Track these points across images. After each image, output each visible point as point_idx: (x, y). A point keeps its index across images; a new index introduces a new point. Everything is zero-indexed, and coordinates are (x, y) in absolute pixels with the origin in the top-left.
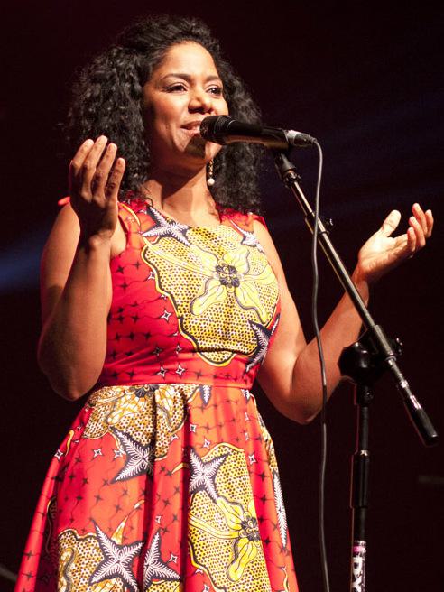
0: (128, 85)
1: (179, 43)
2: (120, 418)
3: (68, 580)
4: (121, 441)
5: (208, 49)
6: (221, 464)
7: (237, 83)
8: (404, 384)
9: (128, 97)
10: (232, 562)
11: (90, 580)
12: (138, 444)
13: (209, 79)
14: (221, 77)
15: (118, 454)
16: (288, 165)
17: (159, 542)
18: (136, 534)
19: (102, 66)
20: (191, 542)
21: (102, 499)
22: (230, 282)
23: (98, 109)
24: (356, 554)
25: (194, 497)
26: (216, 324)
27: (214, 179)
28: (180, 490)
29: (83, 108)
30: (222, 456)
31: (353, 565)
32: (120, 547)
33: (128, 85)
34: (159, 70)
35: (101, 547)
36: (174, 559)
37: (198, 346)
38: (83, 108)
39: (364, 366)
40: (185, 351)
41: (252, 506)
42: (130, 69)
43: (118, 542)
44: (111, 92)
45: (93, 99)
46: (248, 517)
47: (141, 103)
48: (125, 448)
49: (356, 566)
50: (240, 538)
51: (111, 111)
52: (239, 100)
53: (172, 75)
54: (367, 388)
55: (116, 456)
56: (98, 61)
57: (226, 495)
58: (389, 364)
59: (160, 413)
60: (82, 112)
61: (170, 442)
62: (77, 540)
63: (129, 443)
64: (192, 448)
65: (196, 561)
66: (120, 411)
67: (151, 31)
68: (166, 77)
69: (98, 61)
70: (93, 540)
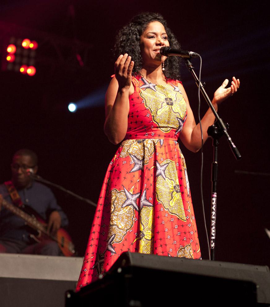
0: (135, 36)
1: (152, 22)
3: (114, 206)
4: (133, 158)
5: (162, 24)
7: (172, 35)
8: (230, 139)
12: (138, 159)
13: (163, 34)
14: (167, 33)
16: (190, 63)
17: (146, 193)
18: (138, 190)
19: (126, 29)
20: (156, 193)
24: (213, 197)
29: (119, 44)
30: (167, 164)
31: (212, 201)
32: (132, 195)
33: (135, 36)
34: (146, 31)
35: (126, 195)
36: (151, 199)
39: (216, 133)
40: (154, 127)
41: (177, 181)
42: (136, 30)
43: (132, 193)
44: (129, 38)
45: (123, 41)
46: (176, 185)
48: (134, 161)
49: (213, 201)
50: (173, 192)
52: (173, 41)
53: (150, 33)
54: (217, 140)
55: (131, 163)
56: (125, 28)
58: (224, 132)
59: (146, 149)
61: (150, 159)
63: (135, 159)
64: (157, 160)
66: (132, 148)
67: (143, 17)
68: (148, 33)
69: (125, 28)
70: (123, 192)
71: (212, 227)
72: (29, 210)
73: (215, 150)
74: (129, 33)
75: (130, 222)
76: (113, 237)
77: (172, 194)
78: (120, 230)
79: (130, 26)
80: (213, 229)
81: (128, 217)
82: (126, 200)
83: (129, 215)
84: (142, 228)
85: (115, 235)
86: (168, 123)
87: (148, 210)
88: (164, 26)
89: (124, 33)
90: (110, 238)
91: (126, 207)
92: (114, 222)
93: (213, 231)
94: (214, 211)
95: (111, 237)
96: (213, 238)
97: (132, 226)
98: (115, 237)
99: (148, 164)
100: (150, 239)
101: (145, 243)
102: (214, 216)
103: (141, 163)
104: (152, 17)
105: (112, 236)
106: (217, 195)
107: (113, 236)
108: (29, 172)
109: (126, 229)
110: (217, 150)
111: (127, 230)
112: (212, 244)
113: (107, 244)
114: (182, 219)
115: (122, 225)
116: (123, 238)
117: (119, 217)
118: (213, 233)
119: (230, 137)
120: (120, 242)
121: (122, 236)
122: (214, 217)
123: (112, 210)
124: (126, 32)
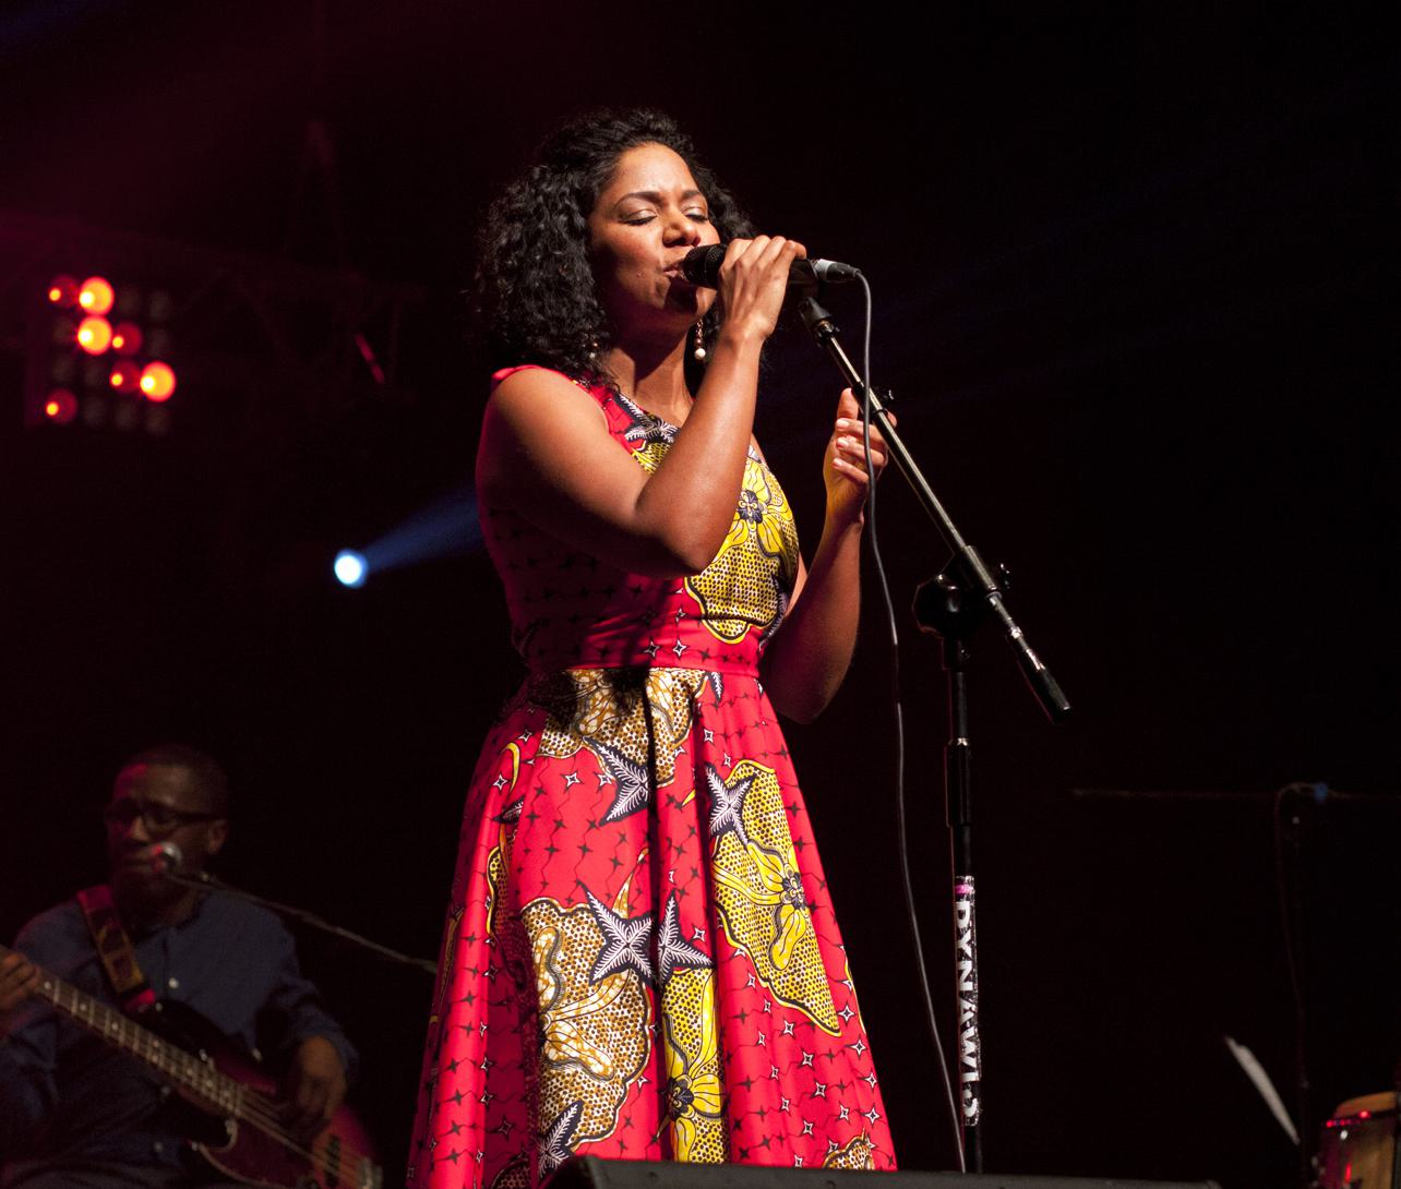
0: (563, 218)
1: (632, 146)
2: (599, 726)
3: (556, 976)
4: (606, 760)
5: (676, 150)
6: (747, 791)
7: (726, 198)
8: (1016, 633)
9: (565, 236)
10: (775, 941)
11: (591, 976)
12: (632, 763)
13: (686, 196)
14: (703, 190)
15: (605, 779)
16: (819, 312)
17: (676, 910)
18: (642, 904)
19: (520, 196)
20: (722, 908)
21: (590, 851)
22: (751, 515)
23: (520, 260)
24: (960, 897)
25: (720, 840)
26: (713, 1132)
27: (706, 350)
28: (699, 872)
29: (496, 261)
30: (746, 779)
31: (956, 914)
32: (627, 922)
33: (563, 218)
34: (611, 191)
35: (600, 924)
36: (700, 934)
37: (706, 611)
38: (496, 261)
39: (953, 609)
40: (688, 618)
41: (791, 855)
42: (564, 194)
43: (623, 914)
44: (539, 232)
45: (513, 245)
46: (790, 872)
47: (587, 244)
48: (613, 769)
49: (961, 914)
50: (781, 905)
51: (542, 259)
52: (732, 222)
53: (632, 195)
54: (960, 643)
55: (602, 783)
56: (513, 190)
57: (757, 838)
58: (991, 604)
59: (656, 714)
60: (497, 268)
61: (676, 758)
62: (560, 914)
63: (617, 762)
64: (708, 764)
65: (733, 937)
66: (598, 713)
67: (590, 134)
68: (623, 199)
69: (513, 190)
70: (585, 915)
71: (964, 1028)
72: (183, 1026)
73: (956, 690)
74: (536, 211)
75: (632, 1042)
76: (570, 1114)
77: (777, 915)
78: (596, 1083)
79: (536, 177)
80: (970, 1039)
81: (622, 1022)
82: (604, 950)
83: (626, 1014)
84: (677, 1067)
85: (580, 1104)
86: (727, 600)
87: (694, 985)
88: (684, 158)
89: (511, 211)
90: (558, 1120)
91: (608, 980)
92: (564, 1047)
93: (971, 1047)
94: (967, 957)
95: (562, 1116)
96: (973, 1077)
97: (643, 1059)
98: (583, 1117)
99: (672, 781)
100: (717, 1110)
101: (698, 1132)
102: (967, 979)
103: (645, 779)
104: (627, 126)
105: (568, 1109)
106: (975, 888)
107: (574, 1110)
108: (164, 856)
109: (622, 1075)
110: (961, 685)
111: (625, 1080)
112: (969, 1103)
113: (543, 1149)
114: (824, 1025)
115: (602, 1061)
116: (614, 1115)
117: (585, 1027)
118: (971, 1055)
119: (1018, 623)
120: (604, 1133)
121: (612, 1107)
122: (968, 986)
123: (549, 994)
124: (520, 205)
